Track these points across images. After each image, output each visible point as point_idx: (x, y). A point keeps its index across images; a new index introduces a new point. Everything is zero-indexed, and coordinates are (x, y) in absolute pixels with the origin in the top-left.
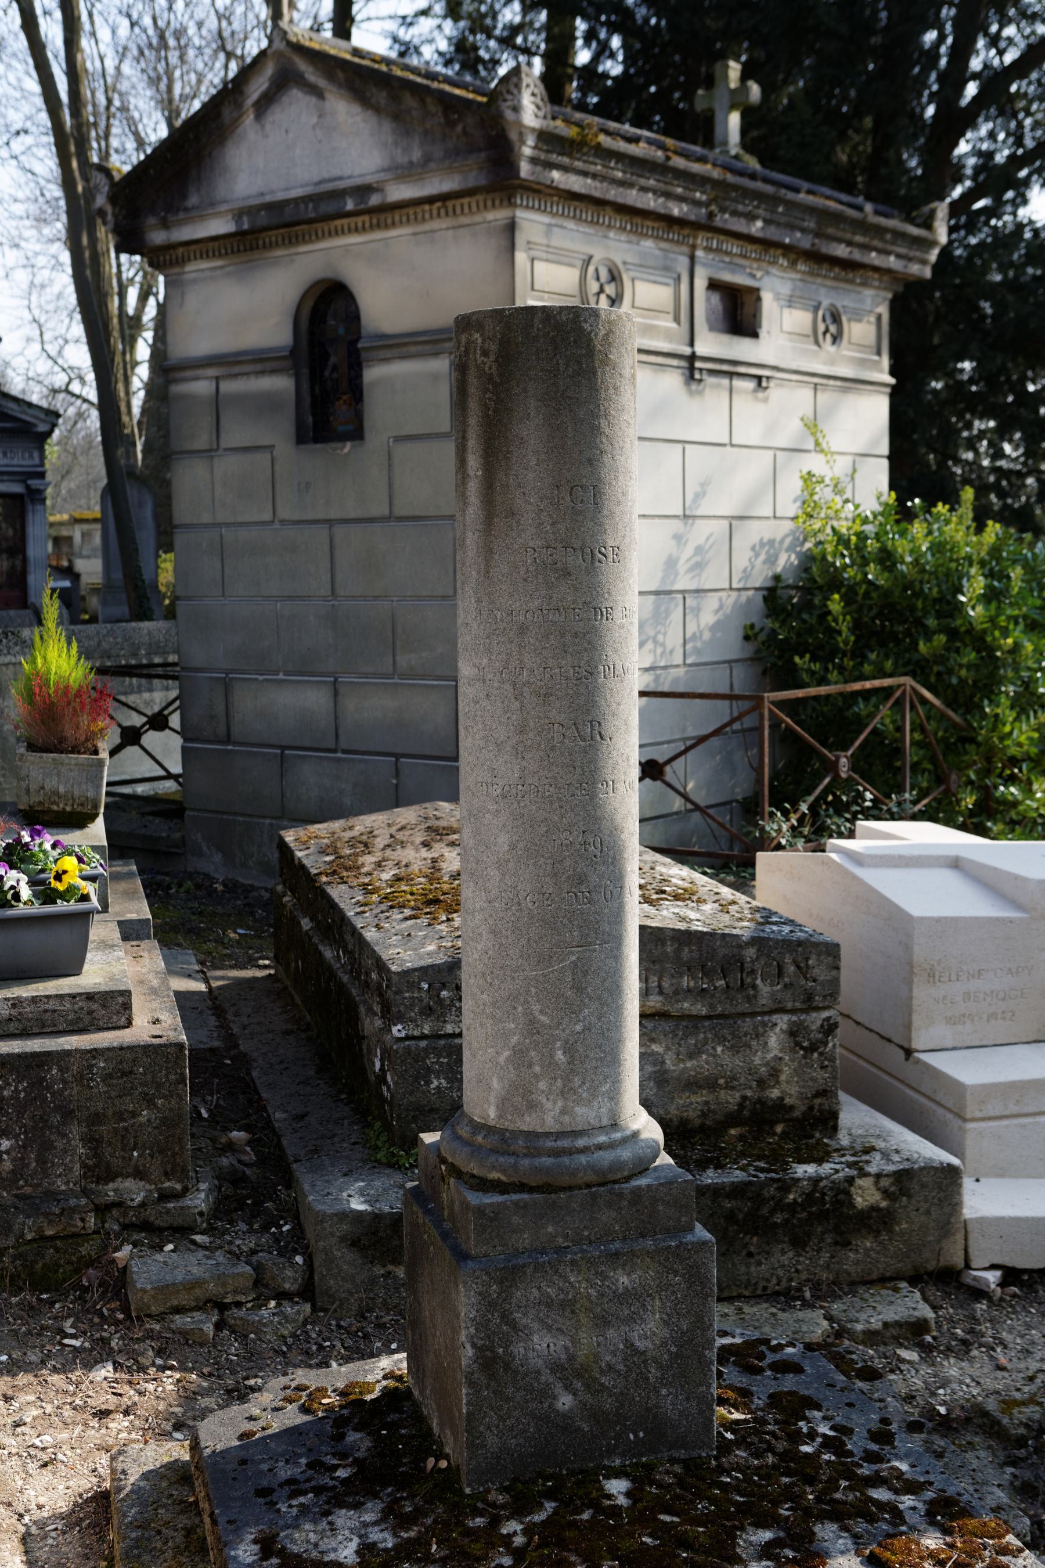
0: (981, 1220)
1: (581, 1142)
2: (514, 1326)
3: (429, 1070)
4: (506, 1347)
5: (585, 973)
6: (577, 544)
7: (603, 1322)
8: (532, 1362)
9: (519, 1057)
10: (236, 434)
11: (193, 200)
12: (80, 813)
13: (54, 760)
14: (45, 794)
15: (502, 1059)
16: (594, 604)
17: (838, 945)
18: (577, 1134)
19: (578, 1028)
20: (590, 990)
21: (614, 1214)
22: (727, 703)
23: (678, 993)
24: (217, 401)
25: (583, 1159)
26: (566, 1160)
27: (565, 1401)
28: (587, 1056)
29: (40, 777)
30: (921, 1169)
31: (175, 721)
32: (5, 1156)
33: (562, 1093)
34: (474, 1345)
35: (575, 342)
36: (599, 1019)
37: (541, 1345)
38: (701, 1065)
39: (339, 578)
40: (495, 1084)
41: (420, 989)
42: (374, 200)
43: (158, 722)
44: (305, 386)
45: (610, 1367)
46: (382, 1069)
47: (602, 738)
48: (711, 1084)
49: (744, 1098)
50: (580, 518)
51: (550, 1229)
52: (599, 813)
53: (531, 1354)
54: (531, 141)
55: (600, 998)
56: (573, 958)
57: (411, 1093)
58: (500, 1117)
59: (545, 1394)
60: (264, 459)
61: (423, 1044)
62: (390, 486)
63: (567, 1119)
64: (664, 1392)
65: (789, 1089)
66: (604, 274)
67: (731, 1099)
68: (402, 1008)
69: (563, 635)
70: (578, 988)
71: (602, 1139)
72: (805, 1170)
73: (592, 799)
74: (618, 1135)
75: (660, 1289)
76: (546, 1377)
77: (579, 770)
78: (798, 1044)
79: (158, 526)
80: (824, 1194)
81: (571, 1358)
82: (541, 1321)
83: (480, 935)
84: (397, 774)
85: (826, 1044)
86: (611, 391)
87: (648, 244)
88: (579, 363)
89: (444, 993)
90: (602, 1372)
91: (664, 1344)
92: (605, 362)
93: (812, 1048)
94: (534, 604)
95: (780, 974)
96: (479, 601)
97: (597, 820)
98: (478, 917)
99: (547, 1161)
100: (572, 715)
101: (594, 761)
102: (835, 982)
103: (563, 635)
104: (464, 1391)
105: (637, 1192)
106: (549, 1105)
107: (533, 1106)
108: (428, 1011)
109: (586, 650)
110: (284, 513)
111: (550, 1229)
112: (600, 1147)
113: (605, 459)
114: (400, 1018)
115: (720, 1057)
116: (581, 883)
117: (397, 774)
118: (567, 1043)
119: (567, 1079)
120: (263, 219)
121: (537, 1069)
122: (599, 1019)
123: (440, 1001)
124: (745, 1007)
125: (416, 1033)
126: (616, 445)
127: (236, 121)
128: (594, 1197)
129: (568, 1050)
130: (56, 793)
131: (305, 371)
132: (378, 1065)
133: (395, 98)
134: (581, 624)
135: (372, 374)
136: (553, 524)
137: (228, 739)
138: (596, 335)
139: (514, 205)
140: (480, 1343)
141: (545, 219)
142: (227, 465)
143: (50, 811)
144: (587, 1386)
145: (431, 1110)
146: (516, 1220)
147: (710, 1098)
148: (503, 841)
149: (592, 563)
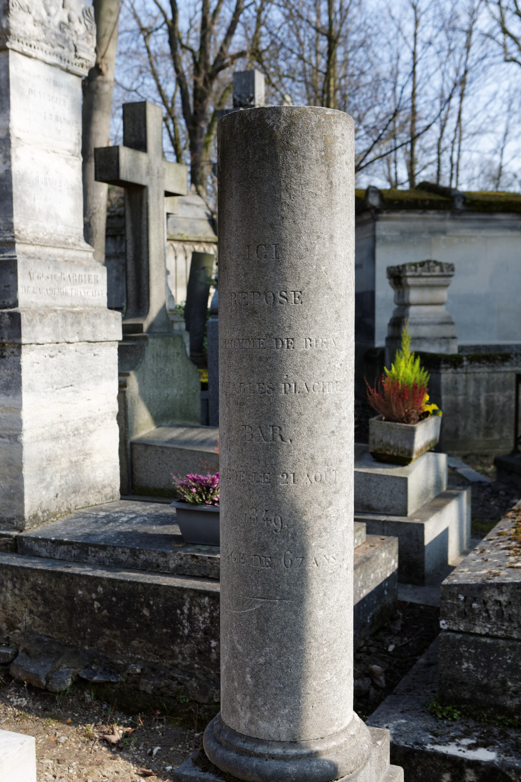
1: (260, 749)
3: (461, 656)
5: (267, 620)
6: (262, 289)
12: (401, 457)
13: (388, 425)
14: (383, 445)
16: (275, 335)
18: (260, 741)
19: (262, 660)
20: (270, 633)
25: (255, 762)
26: (243, 759)
28: (268, 684)
29: (381, 435)
32: (213, 650)
33: (250, 707)
35: (260, 135)
36: (279, 657)
41: (458, 599)
47: (282, 440)
50: (264, 270)
52: (279, 497)
55: (279, 641)
56: (258, 606)
57: (449, 668)
63: (253, 728)
68: (445, 609)
69: (251, 359)
70: (261, 630)
71: (278, 751)
73: (273, 486)
74: (293, 752)
77: (262, 463)
86: (293, 170)
88: (263, 150)
89: (475, 605)
92: (287, 147)
97: (277, 503)
99: (233, 755)
100: (258, 420)
101: (274, 457)
103: (251, 359)
106: (242, 714)
108: (463, 615)
109: (268, 370)
112: (273, 757)
113: (286, 223)
116: (264, 550)
118: (253, 670)
122: (279, 657)
123: (472, 610)
125: (455, 628)
126: (298, 212)
130: (388, 444)
134: (264, 351)
136: (245, 275)
138: (278, 127)
143: (385, 454)
145: (462, 683)
149: (274, 304)
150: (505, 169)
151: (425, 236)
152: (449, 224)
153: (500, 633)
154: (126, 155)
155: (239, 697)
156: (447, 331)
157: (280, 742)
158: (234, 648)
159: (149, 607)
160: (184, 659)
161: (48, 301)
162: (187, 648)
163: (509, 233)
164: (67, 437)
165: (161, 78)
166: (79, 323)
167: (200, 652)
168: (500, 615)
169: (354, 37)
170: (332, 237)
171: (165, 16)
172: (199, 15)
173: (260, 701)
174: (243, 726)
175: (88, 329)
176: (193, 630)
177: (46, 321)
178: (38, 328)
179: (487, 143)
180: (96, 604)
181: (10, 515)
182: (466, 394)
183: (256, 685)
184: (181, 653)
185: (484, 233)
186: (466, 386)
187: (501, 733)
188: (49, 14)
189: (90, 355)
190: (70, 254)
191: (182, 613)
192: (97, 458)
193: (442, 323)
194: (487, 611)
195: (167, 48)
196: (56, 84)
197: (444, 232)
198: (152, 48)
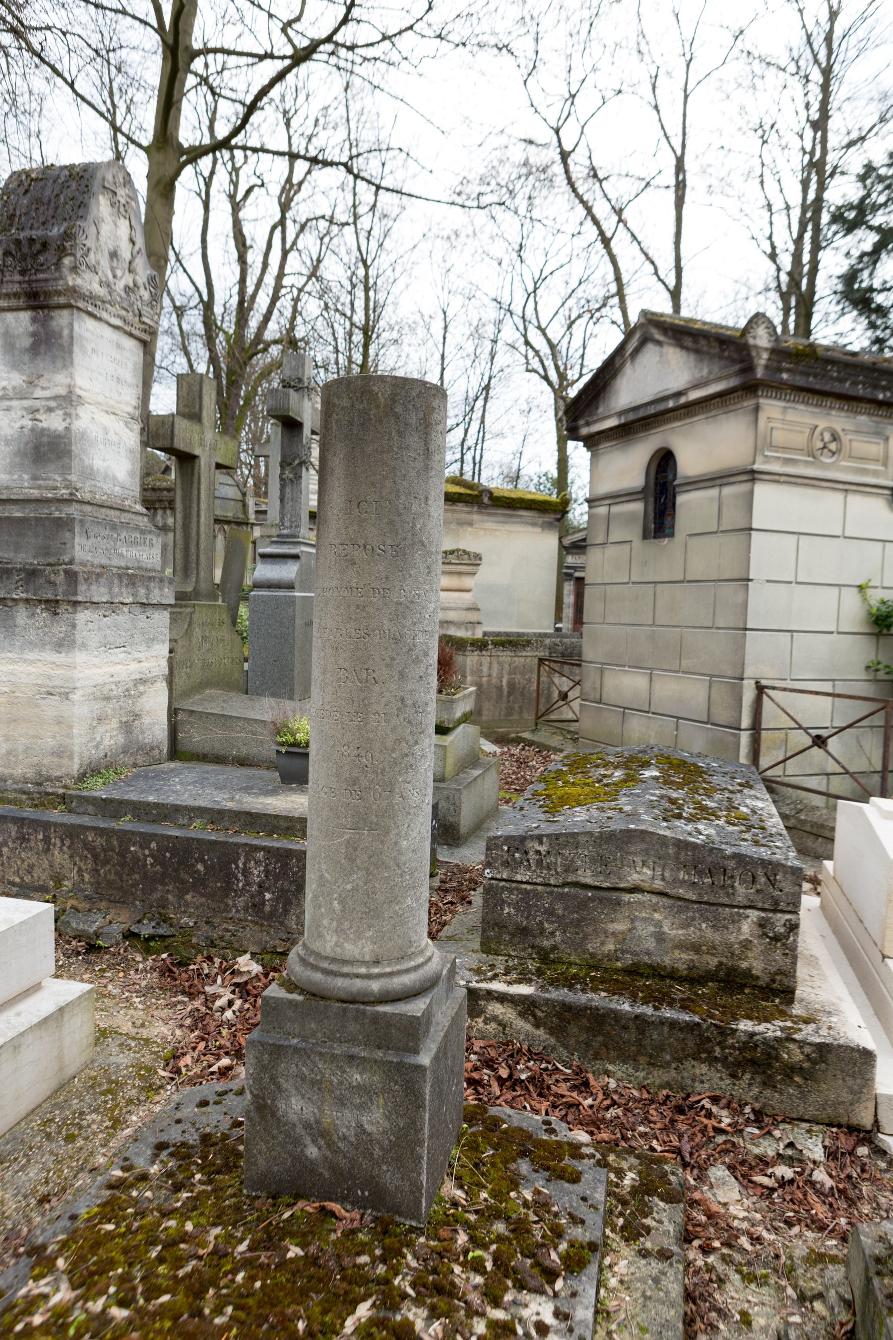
0: (887, 1096)
1: (346, 969)
3: (503, 902)
4: (273, 1100)
5: (355, 849)
10: (615, 536)
11: (601, 410)
18: (345, 962)
19: (349, 887)
22: (830, 699)
23: (676, 882)
30: (840, 1046)
38: (691, 934)
42: (683, 400)
44: (651, 507)
45: (345, 1138)
48: (696, 948)
49: (721, 963)
54: (765, 356)
60: (626, 547)
61: (502, 884)
63: (338, 950)
65: (755, 963)
66: (827, 437)
67: (713, 962)
71: (363, 970)
72: (745, 1025)
76: (299, 1130)
78: (765, 935)
80: (756, 1046)
81: (318, 1122)
85: (787, 938)
87: (863, 418)
95: (754, 880)
108: (506, 864)
110: (634, 579)
112: (358, 976)
115: (705, 931)
119: (340, 923)
120: (631, 417)
123: (514, 860)
124: (726, 900)
127: (623, 365)
128: (345, 1010)
131: (651, 500)
133: (696, 341)
135: (681, 499)
139: (757, 397)
142: (611, 551)
144: (328, 1146)
146: (290, 1013)
147: (695, 957)
150: (522, 472)
151: (453, 526)
152: (476, 517)
153: (539, 880)
154: (182, 424)
155: (325, 922)
156: (473, 617)
157: (364, 963)
158: (322, 877)
159: (203, 861)
160: (237, 911)
161: (104, 561)
162: (241, 902)
163: (530, 529)
164: (118, 698)
165: (193, 358)
166: (134, 584)
167: (254, 905)
168: (539, 863)
169: (385, 336)
170: (427, 498)
171: (200, 296)
172: (235, 299)
173: (346, 924)
174: (328, 949)
175: (142, 591)
176: (248, 884)
177: (102, 580)
178: (94, 587)
179: (510, 444)
180: (150, 860)
181: (59, 774)
182: (490, 675)
184: (235, 906)
185: (507, 527)
186: (490, 668)
188: (115, 276)
189: (143, 617)
190: (125, 517)
191: (237, 867)
192: (146, 720)
193: (468, 609)
195: (200, 328)
196: (118, 346)
197: (471, 524)
198: (185, 327)
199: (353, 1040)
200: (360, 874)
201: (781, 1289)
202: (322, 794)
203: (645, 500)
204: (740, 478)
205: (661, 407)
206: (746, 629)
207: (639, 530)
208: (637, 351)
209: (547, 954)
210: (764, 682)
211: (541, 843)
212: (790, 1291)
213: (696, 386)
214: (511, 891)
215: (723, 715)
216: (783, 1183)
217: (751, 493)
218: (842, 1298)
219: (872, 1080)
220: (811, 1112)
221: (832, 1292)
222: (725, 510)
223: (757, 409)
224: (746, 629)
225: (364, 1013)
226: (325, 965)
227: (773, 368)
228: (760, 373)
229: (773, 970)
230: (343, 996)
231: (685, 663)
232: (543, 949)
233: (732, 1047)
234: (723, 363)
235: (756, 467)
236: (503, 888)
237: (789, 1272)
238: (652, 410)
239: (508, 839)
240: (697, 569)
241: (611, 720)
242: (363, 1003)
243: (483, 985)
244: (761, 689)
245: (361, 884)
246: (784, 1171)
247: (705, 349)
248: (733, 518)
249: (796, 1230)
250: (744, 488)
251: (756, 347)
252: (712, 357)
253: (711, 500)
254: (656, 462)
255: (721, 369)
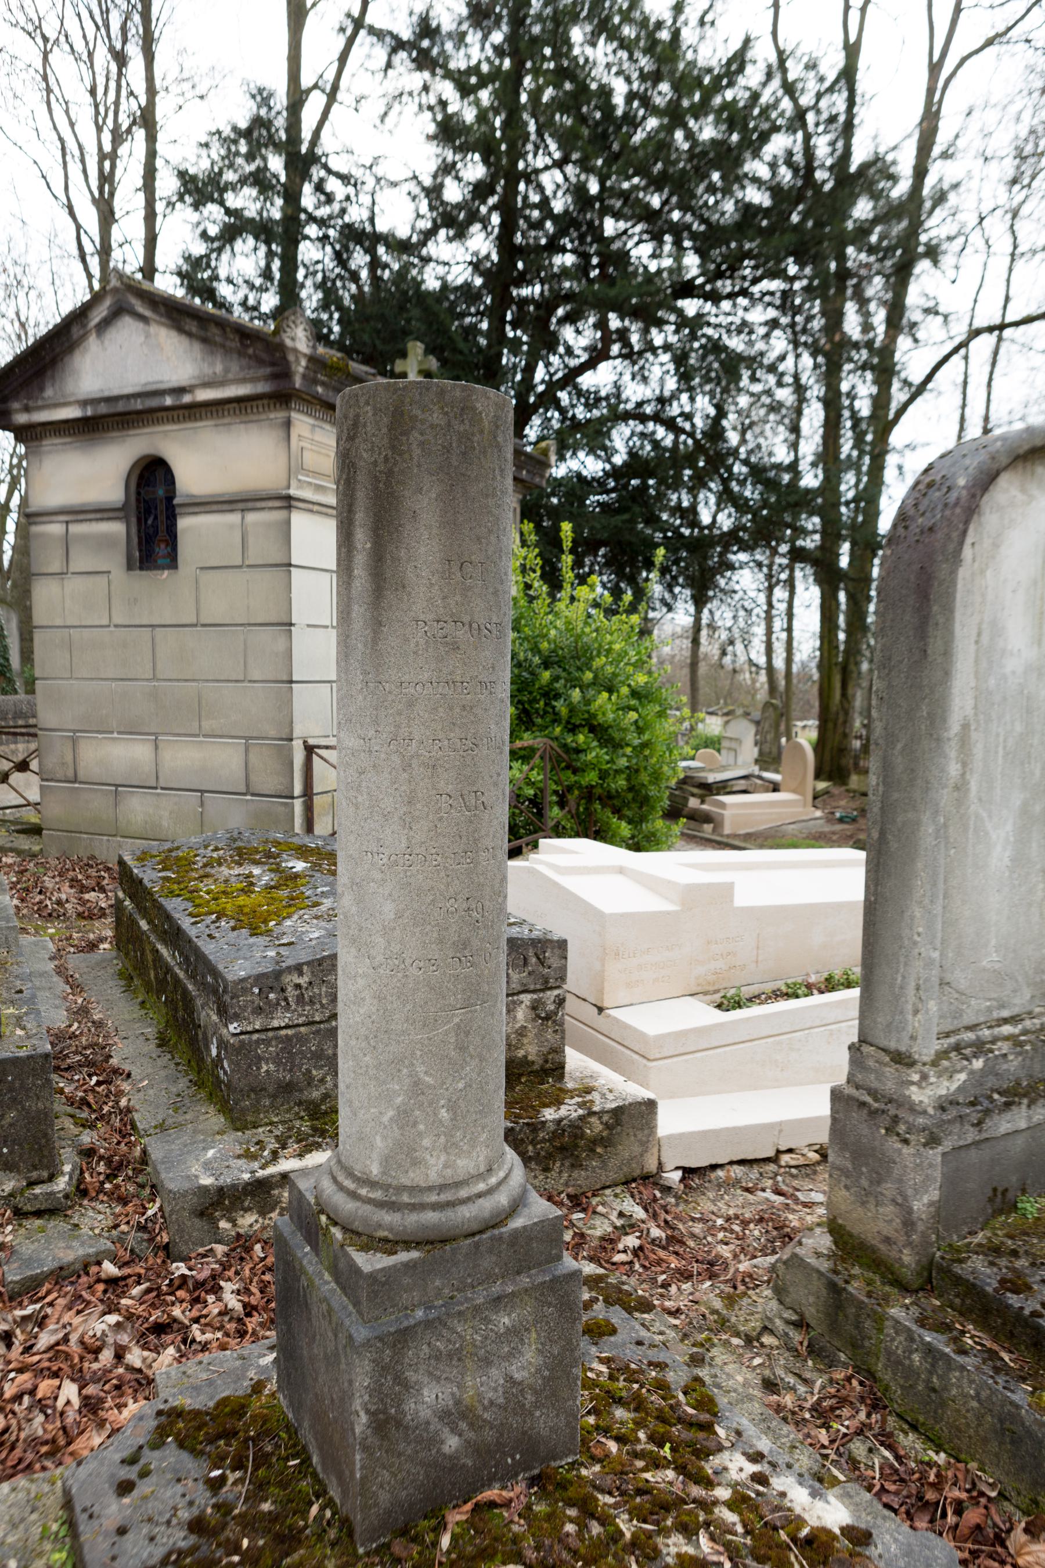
0: (670, 1137)
1: (463, 1193)
2: (406, 1386)
3: (259, 1059)
5: (467, 1034)
7: (487, 1362)
8: (422, 1414)
9: (404, 1118)
10: (80, 562)
11: (49, 392)
15: (385, 1119)
17: (565, 941)
18: (458, 1185)
19: (461, 1085)
21: (494, 1258)
24: (67, 541)
27: (452, 1443)
31: (34, 765)
34: (368, 1412)
37: (429, 1397)
39: (159, 666)
40: (379, 1141)
42: (187, 399)
43: (23, 766)
44: (134, 530)
46: (219, 1055)
51: (437, 1283)
53: (420, 1407)
54: (303, 362)
56: (457, 1020)
58: (384, 1173)
59: (435, 1441)
60: (102, 580)
61: (255, 1037)
62: (197, 601)
64: (538, 1413)
71: (481, 1186)
72: (549, 1114)
75: (536, 1322)
78: (538, 1016)
79: (21, 635)
81: (458, 1402)
82: (430, 1374)
83: (363, 999)
84: (202, 805)
89: (272, 996)
90: (485, 1409)
91: (538, 1371)
93: (547, 1018)
94: (426, 676)
96: (365, 673)
98: (361, 982)
102: (564, 969)
103: (451, 709)
104: (358, 1457)
105: (516, 1233)
106: (432, 1161)
107: (416, 1163)
108: (259, 1011)
110: (118, 619)
111: (437, 1283)
112: (480, 1195)
114: (236, 1017)
117: (202, 805)
119: (449, 1135)
120: (103, 409)
121: (421, 1127)
127: (84, 337)
129: (452, 1108)
132: (214, 1052)
135: (184, 523)
136: (444, 598)
137: (75, 781)
139: (288, 408)
140: (373, 1408)
141: (311, 421)
142: (75, 585)
144: (471, 1425)
146: (406, 1281)
148: (389, 910)
168: (300, 999)
183: (454, 1119)
187: (314, 1129)
194: (286, 999)
199: (490, 1278)
200: (473, 1063)
201: (726, 1343)
202: (413, 971)
203: (127, 520)
204: (270, 504)
205: (154, 403)
206: (291, 682)
207: (121, 558)
208: (106, 323)
209: (317, 1106)
210: (311, 742)
211: (301, 974)
212: (736, 1341)
213: (207, 385)
214: (267, 1042)
215: (267, 781)
216: (637, 1252)
217: (288, 522)
218: (788, 1322)
219: (655, 1127)
220: (612, 1176)
221: (778, 1322)
222: (251, 540)
223: (288, 424)
224: (291, 682)
225: (500, 1238)
226: (433, 1198)
227: (310, 379)
228: (298, 382)
229: (545, 1050)
230: (475, 1227)
231: (207, 725)
232: (312, 1102)
233: (544, 1141)
234: (244, 362)
235: (292, 492)
236: (258, 1041)
237: (723, 1323)
238: (138, 405)
239: (259, 978)
240: (216, 608)
241: (97, 804)
242: (493, 1227)
243: (271, 1170)
244: (310, 750)
245: (474, 1075)
246: (631, 1241)
247: (218, 339)
248: (262, 550)
249: (673, 1289)
250: (278, 515)
251: (295, 350)
252: (227, 351)
253: (231, 527)
254: (137, 472)
255: (242, 368)
